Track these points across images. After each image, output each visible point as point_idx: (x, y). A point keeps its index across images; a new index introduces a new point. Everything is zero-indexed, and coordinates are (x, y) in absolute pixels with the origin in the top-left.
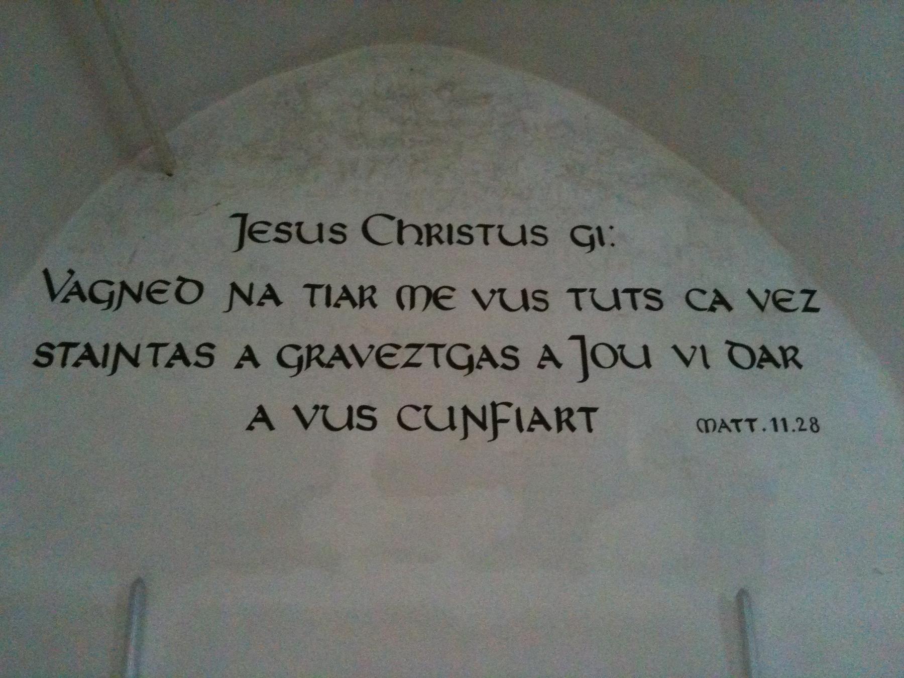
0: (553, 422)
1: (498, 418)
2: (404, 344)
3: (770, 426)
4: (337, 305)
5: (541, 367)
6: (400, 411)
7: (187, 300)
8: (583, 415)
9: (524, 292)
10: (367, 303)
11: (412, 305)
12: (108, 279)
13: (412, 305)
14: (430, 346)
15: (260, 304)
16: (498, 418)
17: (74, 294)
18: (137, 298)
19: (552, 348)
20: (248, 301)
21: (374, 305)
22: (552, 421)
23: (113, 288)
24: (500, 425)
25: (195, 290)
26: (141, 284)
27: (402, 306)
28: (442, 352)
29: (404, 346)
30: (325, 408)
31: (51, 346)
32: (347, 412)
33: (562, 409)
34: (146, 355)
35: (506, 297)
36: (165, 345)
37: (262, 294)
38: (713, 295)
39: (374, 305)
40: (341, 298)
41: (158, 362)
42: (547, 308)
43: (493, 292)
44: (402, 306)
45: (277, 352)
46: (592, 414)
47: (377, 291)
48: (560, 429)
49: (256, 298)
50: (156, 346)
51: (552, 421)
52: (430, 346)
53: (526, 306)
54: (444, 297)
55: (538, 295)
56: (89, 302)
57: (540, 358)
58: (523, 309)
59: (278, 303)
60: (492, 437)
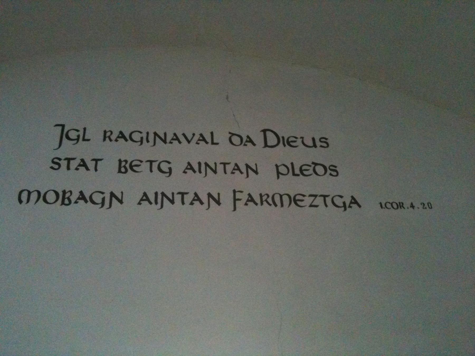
0: (258, 201)
1: (237, 198)
3: (421, 207)
5: (185, 172)
6: (48, 191)
8: (180, 196)
12: (77, 128)
15: (116, 140)
16: (237, 198)
17: (175, 140)
19: (239, 165)
20: (165, 142)
22: (258, 200)
23: (79, 133)
24: (237, 202)
25: (239, 139)
28: (155, 165)
29: (144, 161)
31: (60, 159)
33: (67, 191)
34: (220, 168)
36: (74, 159)
37: (117, 136)
40: (173, 139)
46: (185, 196)
48: (262, 204)
49: (168, 140)
50: (225, 164)
51: (258, 200)
54: (292, 142)
56: (130, 141)
57: (232, 169)
60: (160, 207)
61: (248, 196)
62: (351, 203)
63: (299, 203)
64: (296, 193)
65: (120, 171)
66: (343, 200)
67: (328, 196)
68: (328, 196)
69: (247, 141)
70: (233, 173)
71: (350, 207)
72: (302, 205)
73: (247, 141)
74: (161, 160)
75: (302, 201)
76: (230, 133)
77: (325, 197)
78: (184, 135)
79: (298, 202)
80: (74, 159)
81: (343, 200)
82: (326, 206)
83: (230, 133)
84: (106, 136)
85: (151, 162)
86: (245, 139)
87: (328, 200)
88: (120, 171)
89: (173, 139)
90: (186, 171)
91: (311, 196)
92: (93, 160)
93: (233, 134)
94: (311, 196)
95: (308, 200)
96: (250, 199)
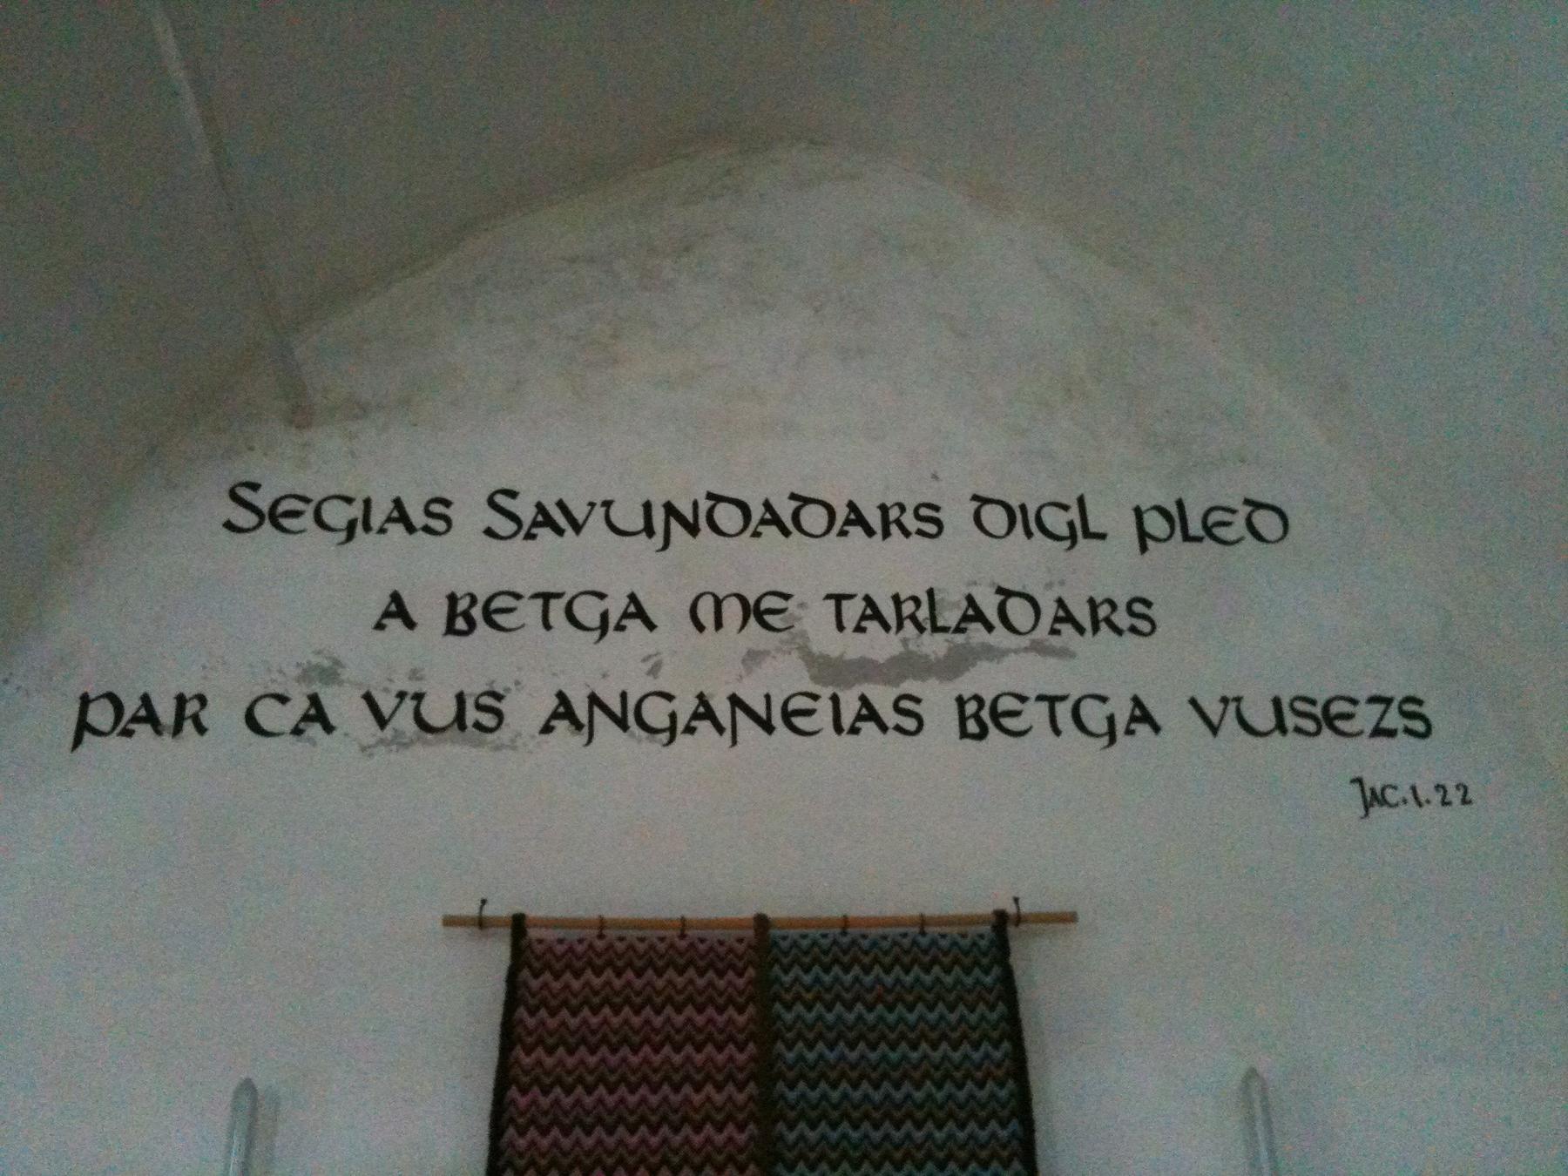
2: (1362, 696)
4: (854, 730)
7: (502, 534)
9: (1277, 702)
10: (188, 726)
11: (719, 624)
13: (719, 624)
14: (1040, 698)
18: (693, 529)
21: (201, 729)
26: (624, 696)
27: (700, 628)
28: (557, 608)
29: (1033, 696)
30: (1238, 700)
32: (454, 702)
35: (1244, 706)
36: (850, 597)
38: (306, 704)
39: (201, 729)
41: (830, 703)
42: (448, 530)
43: (1225, 700)
44: (700, 628)
45: (247, 705)
47: (209, 702)
52: (1040, 698)
53: (1281, 727)
55: (1300, 706)
58: (1143, 508)
59: (410, 624)
61: (697, 701)
62: (696, 716)
63: (799, 722)
64: (1332, 694)
65: (451, 630)
66: (1107, 709)
67: (1063, 698)
68: (1063, 698)
69: (763, 522)
70: (859, 629)
71: (1129, 732)
72: (1023, 727)
73: (763, 522)
74: (575, 592)
75: (1348, 717)
76: (975, 498)
77: (1052, 700)
78: (561, 505)
79: (1339, 724)
80: (850, 597)
81: (1107, 709)
82: (1057, 732)
83: (975, 498)
84: (439, 511)
85: (547, 597)
86: (757, 512)
87: (1063, 710)
88: (451, 630)
89: (389, 520)
90: (864, 624)
91: (1374, 700)
92: (829, 597)
93: (806, 501)
94: (1374, 700)
95: (1367, 716)
96: (561, 710)
